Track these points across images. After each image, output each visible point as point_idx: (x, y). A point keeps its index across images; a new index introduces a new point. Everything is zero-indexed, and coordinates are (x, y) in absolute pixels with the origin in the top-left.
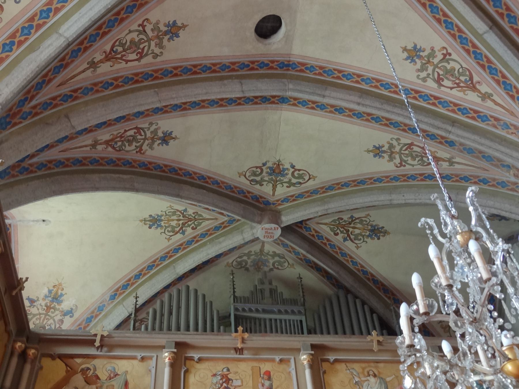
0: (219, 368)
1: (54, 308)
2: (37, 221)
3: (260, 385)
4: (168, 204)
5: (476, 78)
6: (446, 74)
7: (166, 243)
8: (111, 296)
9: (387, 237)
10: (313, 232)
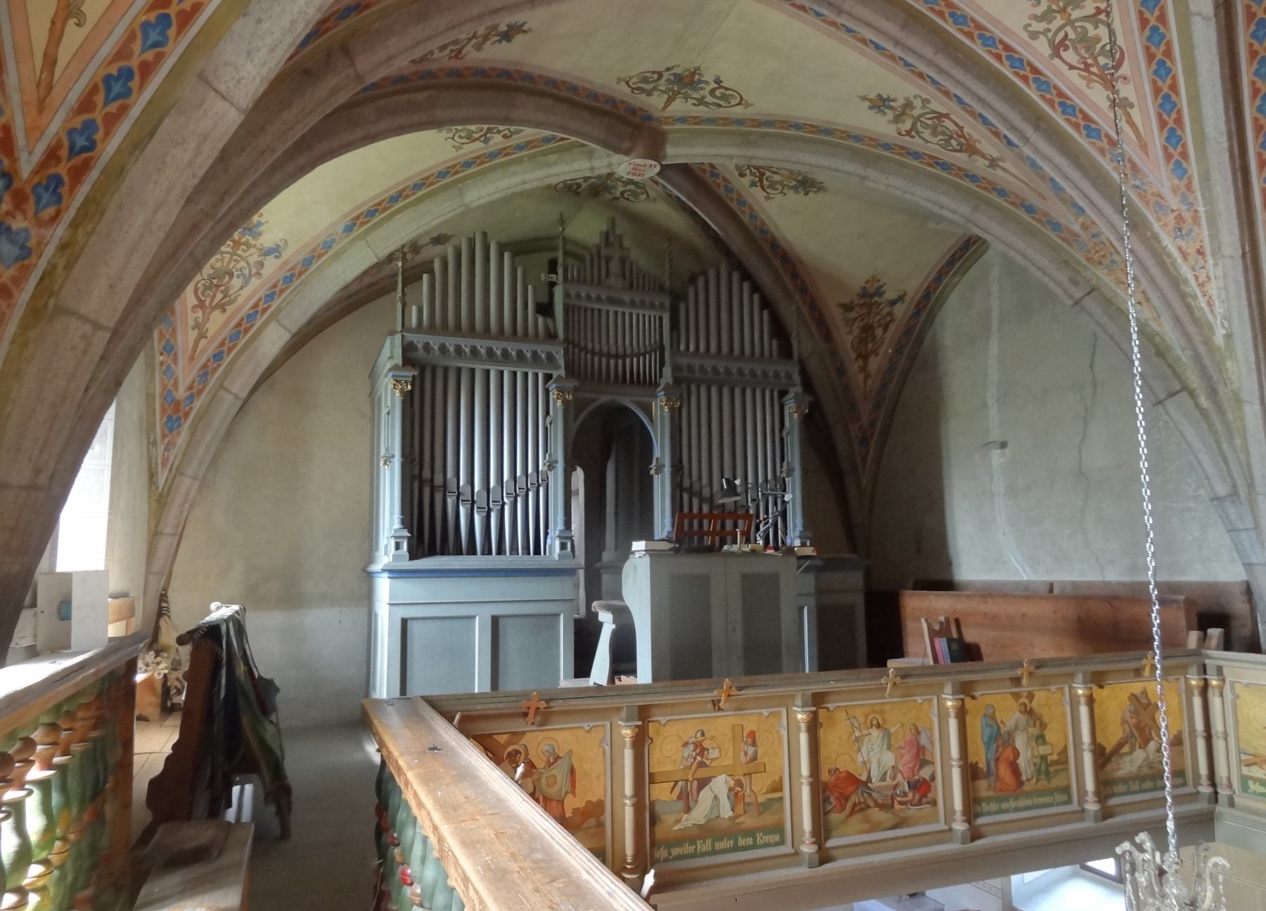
1: (247, 244)
3: (742, 754)
5: (1125, 69)
6: (1080, 41)
7: (453, 153)
9: (821, 194)
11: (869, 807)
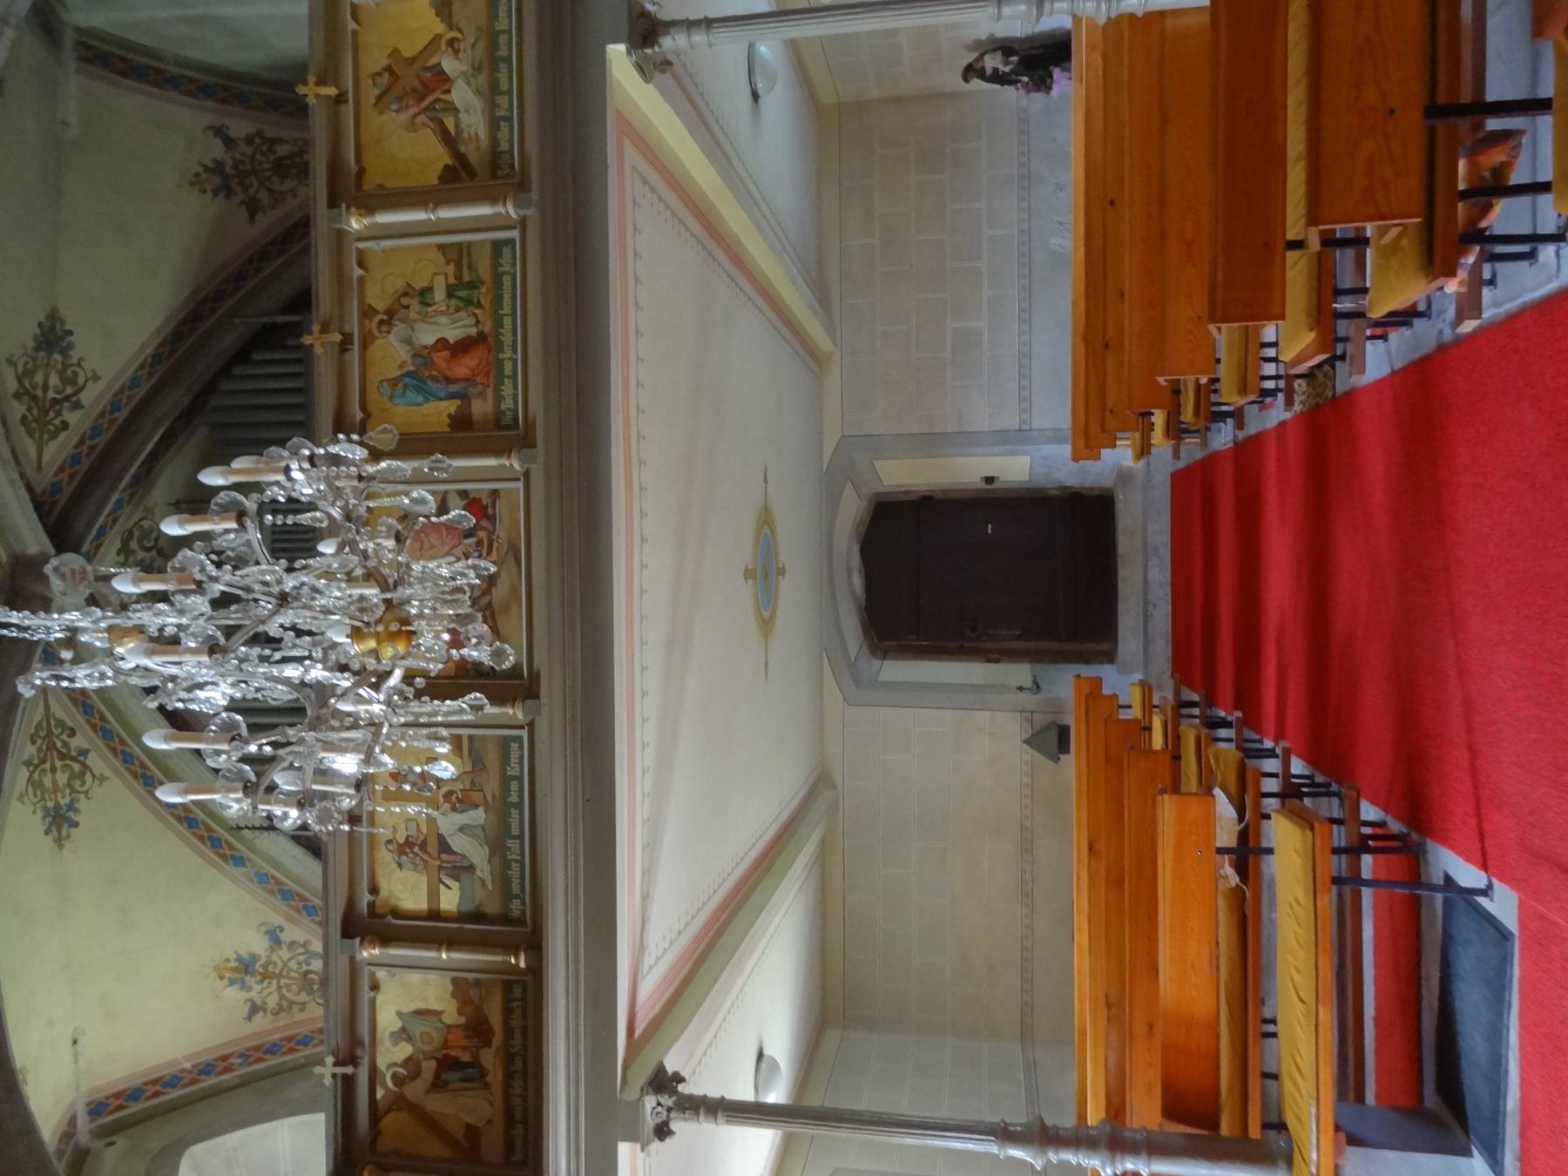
0: (386, 857)
1: (265, 966)
2: (76, 1055)
4: (15, 803)
8: (236, 865)
9: (63, 313)
10: (64, 476)
11: (490, 604)
